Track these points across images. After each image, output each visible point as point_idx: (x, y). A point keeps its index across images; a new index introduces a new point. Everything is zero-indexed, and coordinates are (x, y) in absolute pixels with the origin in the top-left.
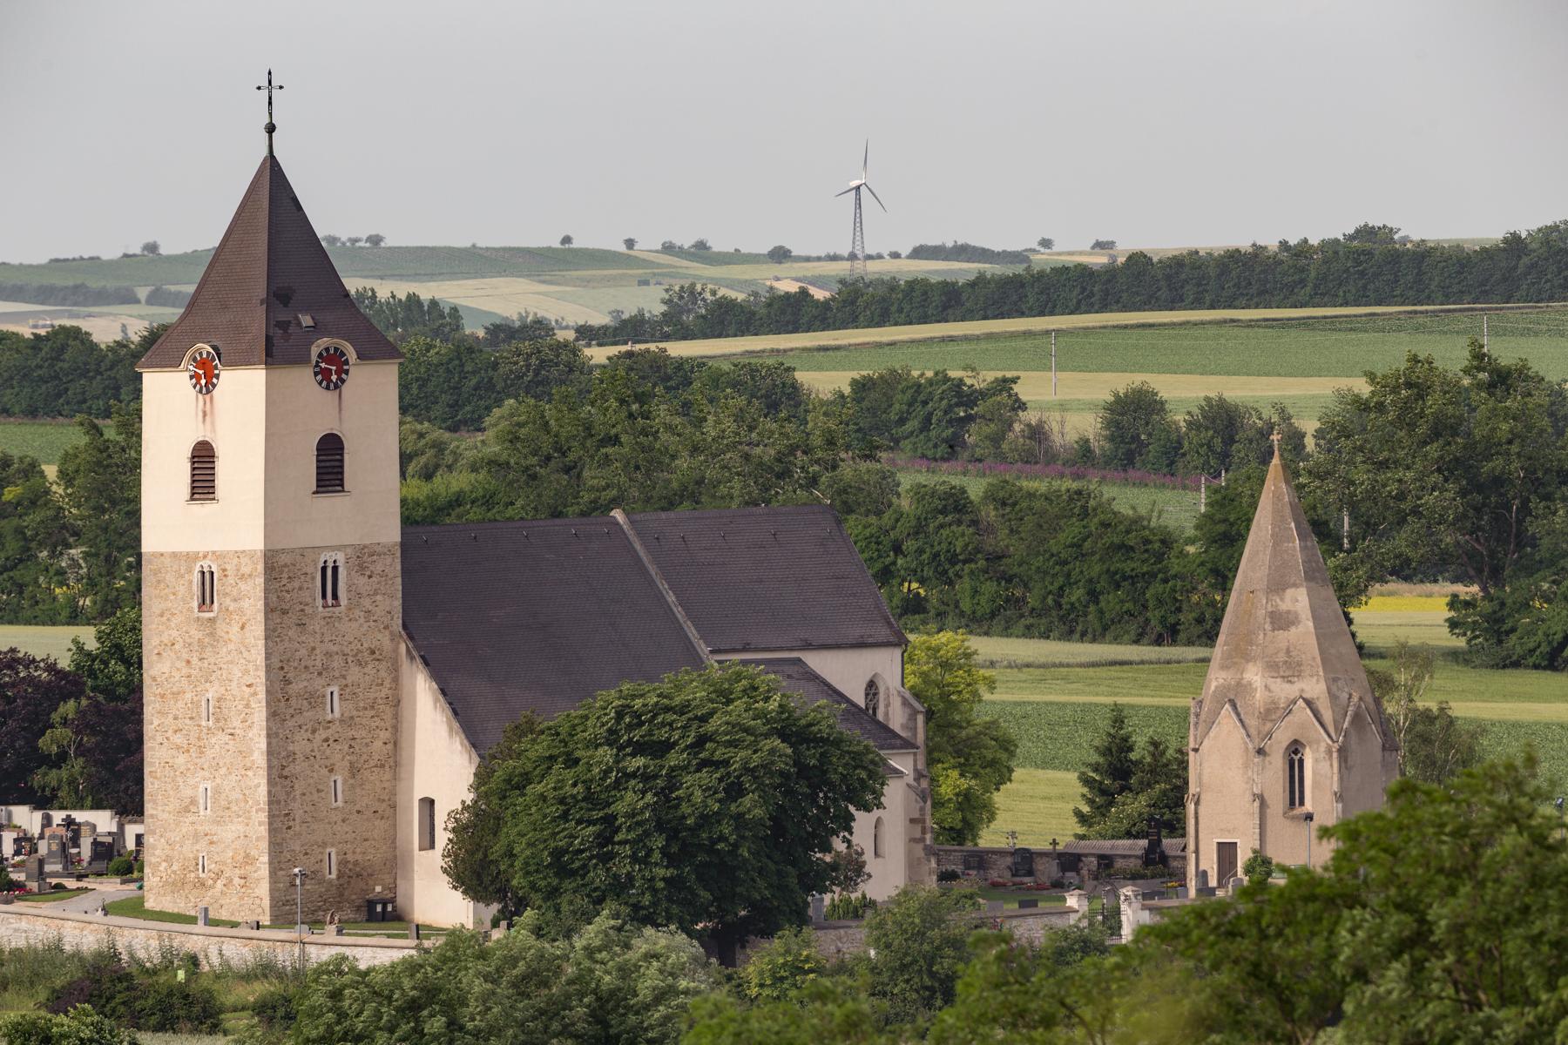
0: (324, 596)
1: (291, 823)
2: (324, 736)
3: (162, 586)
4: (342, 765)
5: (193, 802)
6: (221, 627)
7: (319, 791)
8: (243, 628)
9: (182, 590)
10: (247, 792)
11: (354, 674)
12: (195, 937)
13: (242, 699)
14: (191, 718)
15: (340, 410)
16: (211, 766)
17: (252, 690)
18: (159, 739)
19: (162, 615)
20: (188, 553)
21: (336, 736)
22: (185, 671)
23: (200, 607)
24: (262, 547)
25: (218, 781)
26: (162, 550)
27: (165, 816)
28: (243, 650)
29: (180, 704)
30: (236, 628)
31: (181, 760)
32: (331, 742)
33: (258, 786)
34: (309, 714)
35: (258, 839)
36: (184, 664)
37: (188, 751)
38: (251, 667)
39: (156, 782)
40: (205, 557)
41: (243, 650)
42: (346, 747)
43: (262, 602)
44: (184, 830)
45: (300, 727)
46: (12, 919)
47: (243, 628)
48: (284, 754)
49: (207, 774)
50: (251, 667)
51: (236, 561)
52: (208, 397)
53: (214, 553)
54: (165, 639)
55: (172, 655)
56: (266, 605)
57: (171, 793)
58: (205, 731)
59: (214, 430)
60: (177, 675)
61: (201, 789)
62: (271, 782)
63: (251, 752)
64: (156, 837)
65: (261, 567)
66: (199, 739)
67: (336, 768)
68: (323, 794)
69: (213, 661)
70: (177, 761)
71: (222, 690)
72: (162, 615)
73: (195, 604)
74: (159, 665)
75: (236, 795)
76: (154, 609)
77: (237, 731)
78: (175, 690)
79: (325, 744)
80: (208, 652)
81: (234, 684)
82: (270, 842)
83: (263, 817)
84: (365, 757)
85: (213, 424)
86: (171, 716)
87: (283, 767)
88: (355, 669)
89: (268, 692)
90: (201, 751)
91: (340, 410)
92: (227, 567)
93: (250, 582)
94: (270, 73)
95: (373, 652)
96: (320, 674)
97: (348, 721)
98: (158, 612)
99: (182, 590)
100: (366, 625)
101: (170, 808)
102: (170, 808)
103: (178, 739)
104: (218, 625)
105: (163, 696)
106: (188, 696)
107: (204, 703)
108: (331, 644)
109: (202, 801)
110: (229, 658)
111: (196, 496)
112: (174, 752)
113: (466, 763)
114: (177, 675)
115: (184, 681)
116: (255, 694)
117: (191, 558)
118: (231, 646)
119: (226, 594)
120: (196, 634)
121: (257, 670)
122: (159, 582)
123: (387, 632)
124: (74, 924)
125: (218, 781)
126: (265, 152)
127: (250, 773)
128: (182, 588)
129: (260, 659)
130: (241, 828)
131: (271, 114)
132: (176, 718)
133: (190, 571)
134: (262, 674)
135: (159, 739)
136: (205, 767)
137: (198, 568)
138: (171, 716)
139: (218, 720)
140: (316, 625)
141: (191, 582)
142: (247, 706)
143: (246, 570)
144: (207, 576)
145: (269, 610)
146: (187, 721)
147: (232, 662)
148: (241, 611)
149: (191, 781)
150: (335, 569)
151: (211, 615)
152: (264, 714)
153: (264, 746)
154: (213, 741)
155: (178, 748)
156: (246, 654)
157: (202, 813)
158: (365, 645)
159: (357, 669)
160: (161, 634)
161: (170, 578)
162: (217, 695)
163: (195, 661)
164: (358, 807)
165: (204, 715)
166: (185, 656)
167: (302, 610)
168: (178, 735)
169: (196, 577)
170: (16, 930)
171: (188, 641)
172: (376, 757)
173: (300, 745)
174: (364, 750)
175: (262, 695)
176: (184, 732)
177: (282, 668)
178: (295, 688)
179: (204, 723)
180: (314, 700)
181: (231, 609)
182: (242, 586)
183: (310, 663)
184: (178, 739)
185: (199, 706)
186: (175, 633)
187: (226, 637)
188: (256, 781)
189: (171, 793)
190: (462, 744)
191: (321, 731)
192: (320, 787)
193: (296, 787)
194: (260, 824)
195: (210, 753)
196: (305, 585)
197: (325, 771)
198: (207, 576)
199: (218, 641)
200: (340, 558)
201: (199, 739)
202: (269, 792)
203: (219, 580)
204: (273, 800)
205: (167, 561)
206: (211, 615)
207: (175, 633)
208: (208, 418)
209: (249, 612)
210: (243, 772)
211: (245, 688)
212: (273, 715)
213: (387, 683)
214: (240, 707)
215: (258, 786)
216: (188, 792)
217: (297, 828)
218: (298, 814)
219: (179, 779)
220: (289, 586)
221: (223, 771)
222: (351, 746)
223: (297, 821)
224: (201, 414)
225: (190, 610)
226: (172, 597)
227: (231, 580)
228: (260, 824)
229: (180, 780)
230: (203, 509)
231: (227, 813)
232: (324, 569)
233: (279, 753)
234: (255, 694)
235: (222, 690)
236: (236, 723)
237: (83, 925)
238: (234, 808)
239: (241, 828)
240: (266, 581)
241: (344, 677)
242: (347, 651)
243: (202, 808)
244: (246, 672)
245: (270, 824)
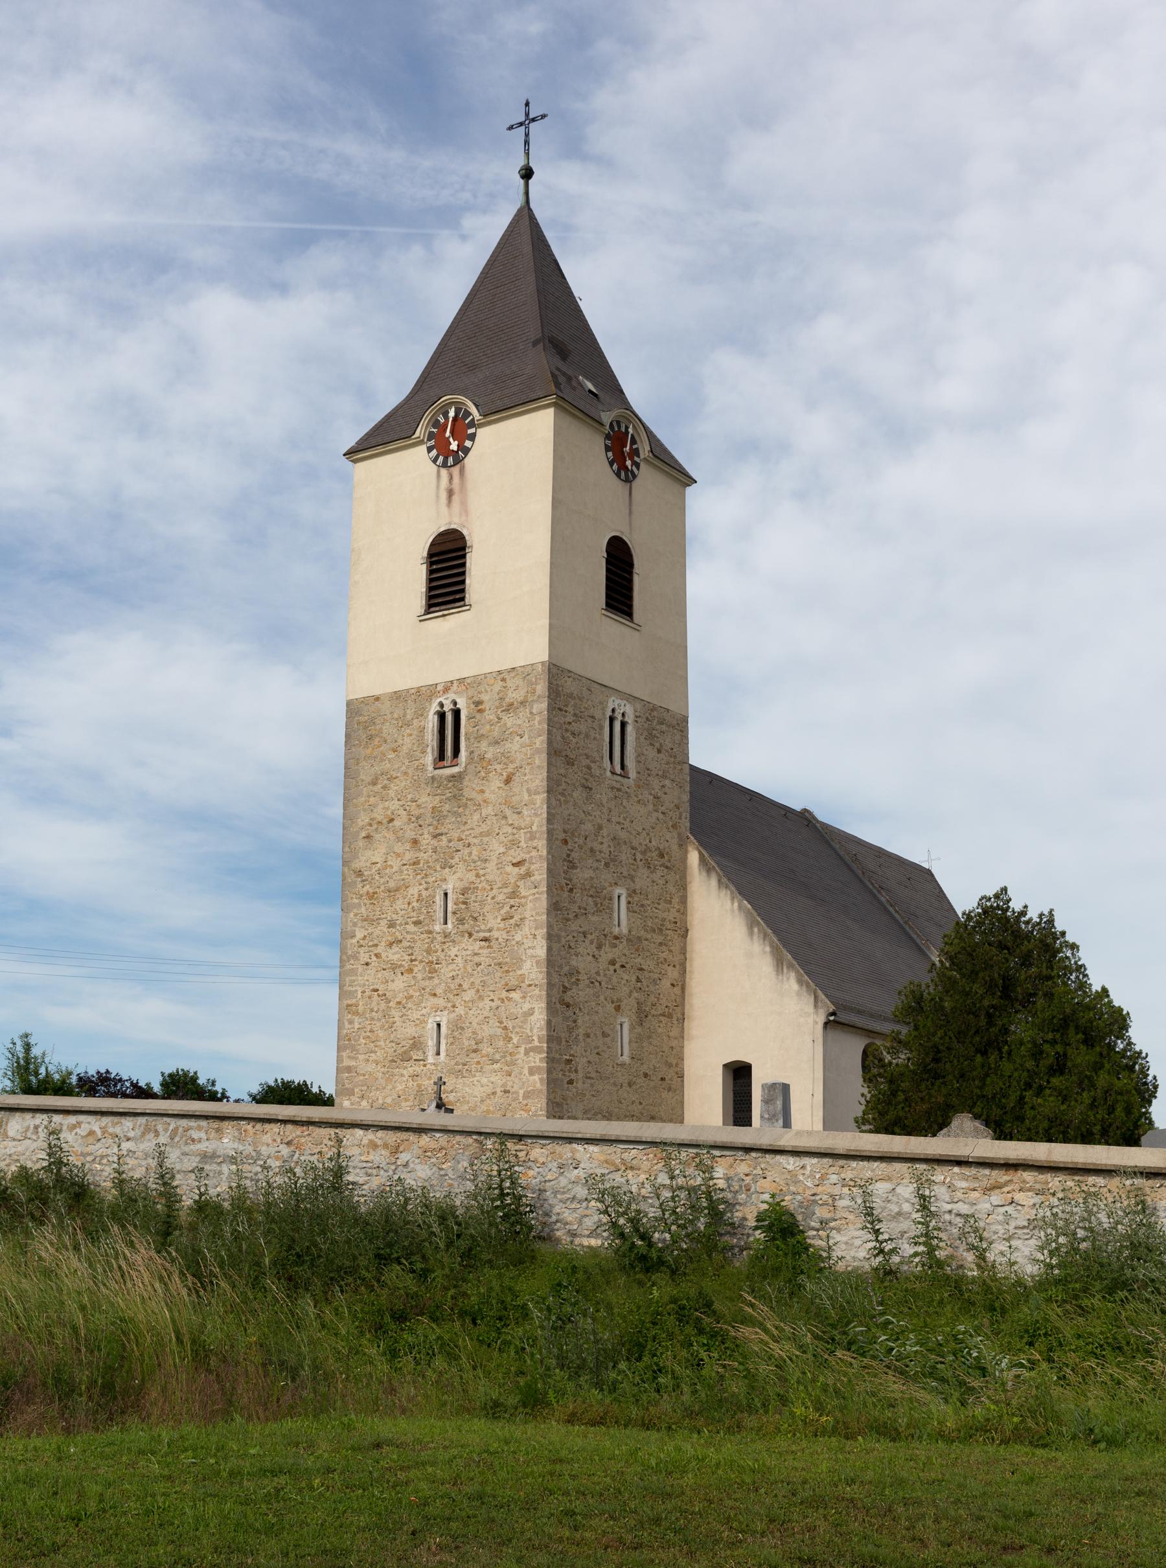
0: (623, 725)
1: (573, 1076)
2: (610, 956)
3: (376, 741)
4: (629, 1005)
5: (417, 1044)
6: (471, 786)
7: (605, 1035)
8: (508, 781)
9: (407, 743)
10: (510, 1025)
11: (643, 878)
12: (791, 1163)
13: (505, 885)
14: (417, 923)
15: (630, 513)
16: (448, 990)
17: (523, 870)
18: (364, 957)
19: (374, 783)
20: (419, 690)
21: (623, 960)
22: (409, 856)
23: (435, 763)
24: (545, 658)
25: (460, 1010)
26: (377, 692)
27: (371, 1067)
28: (508, 812)
29: (400, 904)
30: (496, 783)
31: (399, 983)
32: (617, 966)
33: (531, 1012)
34: (594, 919)
35: (527, 1096)
36: (408, 846)
37: (410, 971)
38: (522, 836)
39: (356, 1019)
40: (446, 690)
41: (508, 812)
42: (634, 979)
43: (544, 737)
44: (400, 1087)
45: (585, 934)
46: (198, 1130)
47: (508, 781)
48: (566, 969)
49: (441, 1002)
50: (522, 836)
51: (498, 685)
52: (456, 471)
53: (461, 681)
54: (379, 814)
55: (390, 836)
56: (550, 742)
57: (381, 1033)
58: (440, 938)
59: (465, 510)
60: (396, 864)
61: (431, 1025)
62: (551, 1009)
63: (519, 962)
64: (355, 1099)
65: (542, 688)
66: (429, 951)
67: (623, 1005)
68: (608, 1040)
69: (455, 835)
70: (391, 986)
71: (471, 876)
72: (374, 783)
73: (429, 758)
74: (369, 853)
75: (487, 1031)
76: (362, 777)
77: (495, 934)
78: (392, 884)
79: (612, 968)
80: (449, 825)
81: (491, 866)
82: (549, 1100)
83: (538, 1060)
84: (652, 999)
85: (464, 503)
86: (383, 923)
87: (565, 989)
88: (643, 872)
89: (550, 871)
90: (432, 969)
91: (630, 513)
92: (485, 697)
93: (524, 713)
94: (527, 104)
95: (662, 856)
96: (607, 865)
97: (634, 941)
98: (369, 779)
99: (407, 743)
100: (655, 815)
101: (380, 1054)
102: (380, 1054)
103: (395, 955)
104: (465, 783)
105: (371, 896)
106: (414, 891)
107: (439, 899)
108: (618, 827)
109: (431, 1043)
110: (484, 828)
111: (433, 609)
112: (388, 974)
113: (810, 1008)
114: (396, 864)
115: (408, 872)
116: (528, 874)
117: (423, 694)
118: (488, 811)
119: (480, 738)
120: (427, 800)
121: (532, 838)
122: (371, 738)
123: (675, 834)
124: (370, 1135)
125: (460, 1010)
126: (519, 202)
127: (515, 995)
128: (407, 740)
129: (539, 823)
130: (498, 1080)
131: (527, 154)
132: (392, 925)
133: (421, 714)
134: (542, 844)
135: (364, 957)
136: (439, 991)
137: (435, 707)
138: (383, 923)
139: (461, 921)
140: (603, 794)
141: (422, 730)
142: (514, 894)
143: (514, 696)
144: (449, 718)
145: (554, 752)
146: (411, 928)
147: (488, 834)
148: (507, 758)
149: (415, 1015)
150: (457, 713)
151: (455, 770)
152: (543, 903)
153: (541, 952)
154: (454, 951)
155: (394, 967)
156: (512, 818)
157: (431, 1059)
158: (654, 843)
159: (645, 872)
160: (372, 808)
161: (388, 729)
162: (460, 885)
163: (426, 839)
164: (644, 1068)
165: (440, 915)
166: (410, 834)
167: (589, 768)
168: (395, 948)
169: (432, 721)
170: (205, 1157)
171: (416, 812)
172: (664, 1001)
173: (583, 963)
174: (652, 988)
175: (540, 874)
176: (405, 944)
177: (565, 842)
178: (582, 875)
179: (438, 928)
180: (602, 902)
181: (489, 756)
182: (509, 721)
183: (597, 847)
184: (395, 955)
185: (430, 902)
186: (394, 805)
187: (479, 798)
188: (526, 1007)
189: (381, 1033)
190: (800, 981)
191: (607, 948)
192: (606, 1029)
193: (580, 1022)
194: (532, 1072)
195: (446, 971)
196: (592, 733)
197: (610, 1007)
198: (449, 718)
199: (466, 806)
200: (629, 710)
201: (429, 951)
202: (549, 1022)
203: (469, 718)
204: (553, 1038)
205: (385, 707)
206: (455, 770)
207: (394, 805)
208: (456, 498)
209: (519, 756)
210: (504, 994)
211: (510, 869)
212: (554, 907)
213: (676, 900)
214: (501, 898)
215: (531, 1012)
216: (411, 1031)
217: (580, 1085)
218: (581, 1062)
219: (393, 1012)
220: (575, 727)
221: (469, 995)
222: (638, 980)
223: (581, 1075)
224: (444, 495)
225: (422, 768)
226: (392, 755)
227: (489, 715)
228: (532, 1072)
229: (396, 1014)
230: (450, 623)
231: (475, 1057)
232: (612, 720)
233: (561, 967)
234: (528, 874)
235: (471, 876)
236: (493, 921)
237: (392, 1137)
238: (486, 1049)
239: (498, 1080)
240: (551, 709)
241: (632, 878)
242: (635, 843)
243: (431, 1052)
244: (515, 843)
245: (549, 1071)
